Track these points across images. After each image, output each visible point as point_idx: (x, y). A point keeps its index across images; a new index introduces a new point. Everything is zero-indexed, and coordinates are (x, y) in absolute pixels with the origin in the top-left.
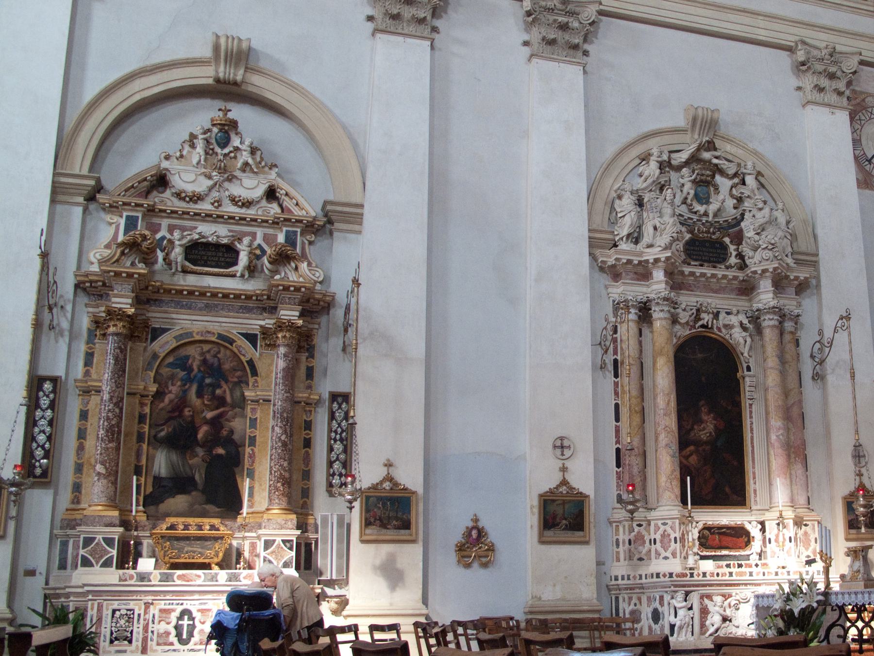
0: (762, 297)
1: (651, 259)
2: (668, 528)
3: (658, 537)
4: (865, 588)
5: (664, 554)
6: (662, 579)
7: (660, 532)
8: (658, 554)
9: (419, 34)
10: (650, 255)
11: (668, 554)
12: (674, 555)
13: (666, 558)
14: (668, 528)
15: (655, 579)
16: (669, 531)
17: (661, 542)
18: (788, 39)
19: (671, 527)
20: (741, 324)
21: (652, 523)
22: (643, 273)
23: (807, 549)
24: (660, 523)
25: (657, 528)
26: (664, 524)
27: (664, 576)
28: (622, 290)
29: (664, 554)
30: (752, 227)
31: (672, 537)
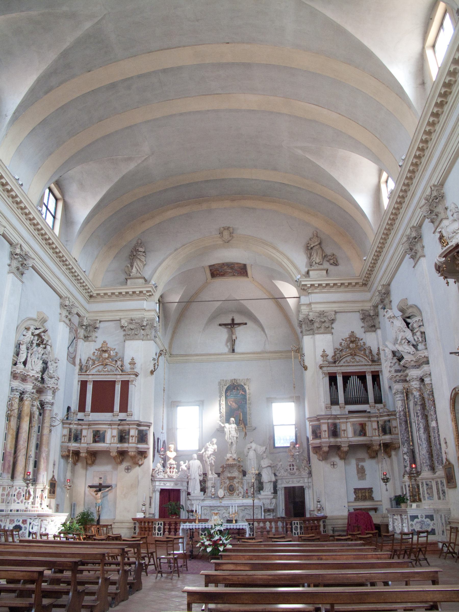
0: (48, 397)
1: (31, 375)
2: (21, 490)
3: (16, 493)
4: (410, 516)
5: (17, 501)
6: (13, 512)
7: (17, 491)
8: (15, 501)
9: (343, 602)
10: (31, 373)
11: (19, 501)
12: (22, 502)
13: (18, 503)
14: (21, 490)
15: (16, 513)
16: (21, 491)
17: (17, 496)
18: (64, 293)
19: (22, 490)
20: (247, 514)
21: (14, 487)
22: (24, 379)
23: (18, 500)
24: (17, 487)
25: (16, 490)
26: (20, 488)
27: (14, 511)
28: (16, 384)
29: (17, 501)
30: (53, 369)
31: (22, 494)
